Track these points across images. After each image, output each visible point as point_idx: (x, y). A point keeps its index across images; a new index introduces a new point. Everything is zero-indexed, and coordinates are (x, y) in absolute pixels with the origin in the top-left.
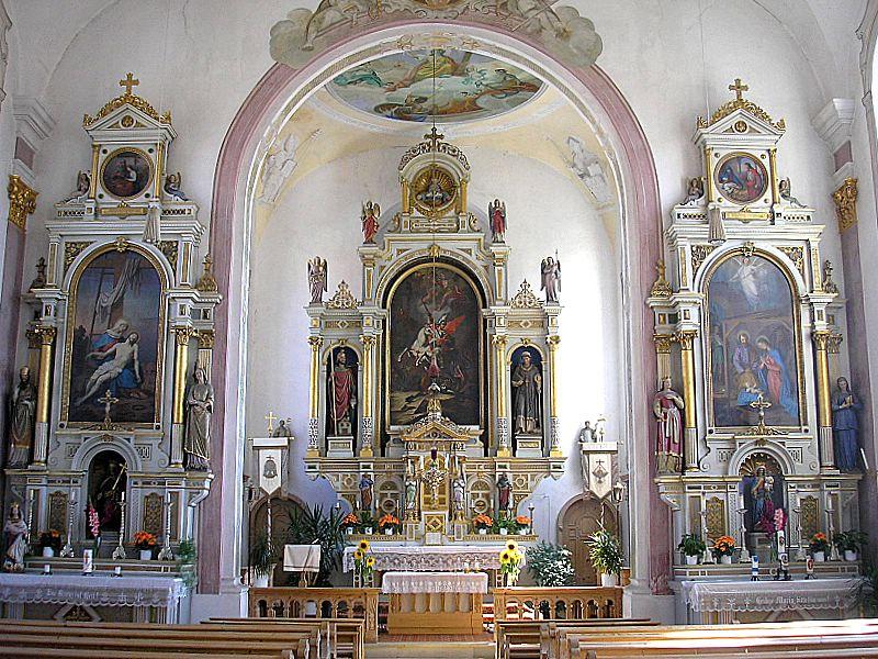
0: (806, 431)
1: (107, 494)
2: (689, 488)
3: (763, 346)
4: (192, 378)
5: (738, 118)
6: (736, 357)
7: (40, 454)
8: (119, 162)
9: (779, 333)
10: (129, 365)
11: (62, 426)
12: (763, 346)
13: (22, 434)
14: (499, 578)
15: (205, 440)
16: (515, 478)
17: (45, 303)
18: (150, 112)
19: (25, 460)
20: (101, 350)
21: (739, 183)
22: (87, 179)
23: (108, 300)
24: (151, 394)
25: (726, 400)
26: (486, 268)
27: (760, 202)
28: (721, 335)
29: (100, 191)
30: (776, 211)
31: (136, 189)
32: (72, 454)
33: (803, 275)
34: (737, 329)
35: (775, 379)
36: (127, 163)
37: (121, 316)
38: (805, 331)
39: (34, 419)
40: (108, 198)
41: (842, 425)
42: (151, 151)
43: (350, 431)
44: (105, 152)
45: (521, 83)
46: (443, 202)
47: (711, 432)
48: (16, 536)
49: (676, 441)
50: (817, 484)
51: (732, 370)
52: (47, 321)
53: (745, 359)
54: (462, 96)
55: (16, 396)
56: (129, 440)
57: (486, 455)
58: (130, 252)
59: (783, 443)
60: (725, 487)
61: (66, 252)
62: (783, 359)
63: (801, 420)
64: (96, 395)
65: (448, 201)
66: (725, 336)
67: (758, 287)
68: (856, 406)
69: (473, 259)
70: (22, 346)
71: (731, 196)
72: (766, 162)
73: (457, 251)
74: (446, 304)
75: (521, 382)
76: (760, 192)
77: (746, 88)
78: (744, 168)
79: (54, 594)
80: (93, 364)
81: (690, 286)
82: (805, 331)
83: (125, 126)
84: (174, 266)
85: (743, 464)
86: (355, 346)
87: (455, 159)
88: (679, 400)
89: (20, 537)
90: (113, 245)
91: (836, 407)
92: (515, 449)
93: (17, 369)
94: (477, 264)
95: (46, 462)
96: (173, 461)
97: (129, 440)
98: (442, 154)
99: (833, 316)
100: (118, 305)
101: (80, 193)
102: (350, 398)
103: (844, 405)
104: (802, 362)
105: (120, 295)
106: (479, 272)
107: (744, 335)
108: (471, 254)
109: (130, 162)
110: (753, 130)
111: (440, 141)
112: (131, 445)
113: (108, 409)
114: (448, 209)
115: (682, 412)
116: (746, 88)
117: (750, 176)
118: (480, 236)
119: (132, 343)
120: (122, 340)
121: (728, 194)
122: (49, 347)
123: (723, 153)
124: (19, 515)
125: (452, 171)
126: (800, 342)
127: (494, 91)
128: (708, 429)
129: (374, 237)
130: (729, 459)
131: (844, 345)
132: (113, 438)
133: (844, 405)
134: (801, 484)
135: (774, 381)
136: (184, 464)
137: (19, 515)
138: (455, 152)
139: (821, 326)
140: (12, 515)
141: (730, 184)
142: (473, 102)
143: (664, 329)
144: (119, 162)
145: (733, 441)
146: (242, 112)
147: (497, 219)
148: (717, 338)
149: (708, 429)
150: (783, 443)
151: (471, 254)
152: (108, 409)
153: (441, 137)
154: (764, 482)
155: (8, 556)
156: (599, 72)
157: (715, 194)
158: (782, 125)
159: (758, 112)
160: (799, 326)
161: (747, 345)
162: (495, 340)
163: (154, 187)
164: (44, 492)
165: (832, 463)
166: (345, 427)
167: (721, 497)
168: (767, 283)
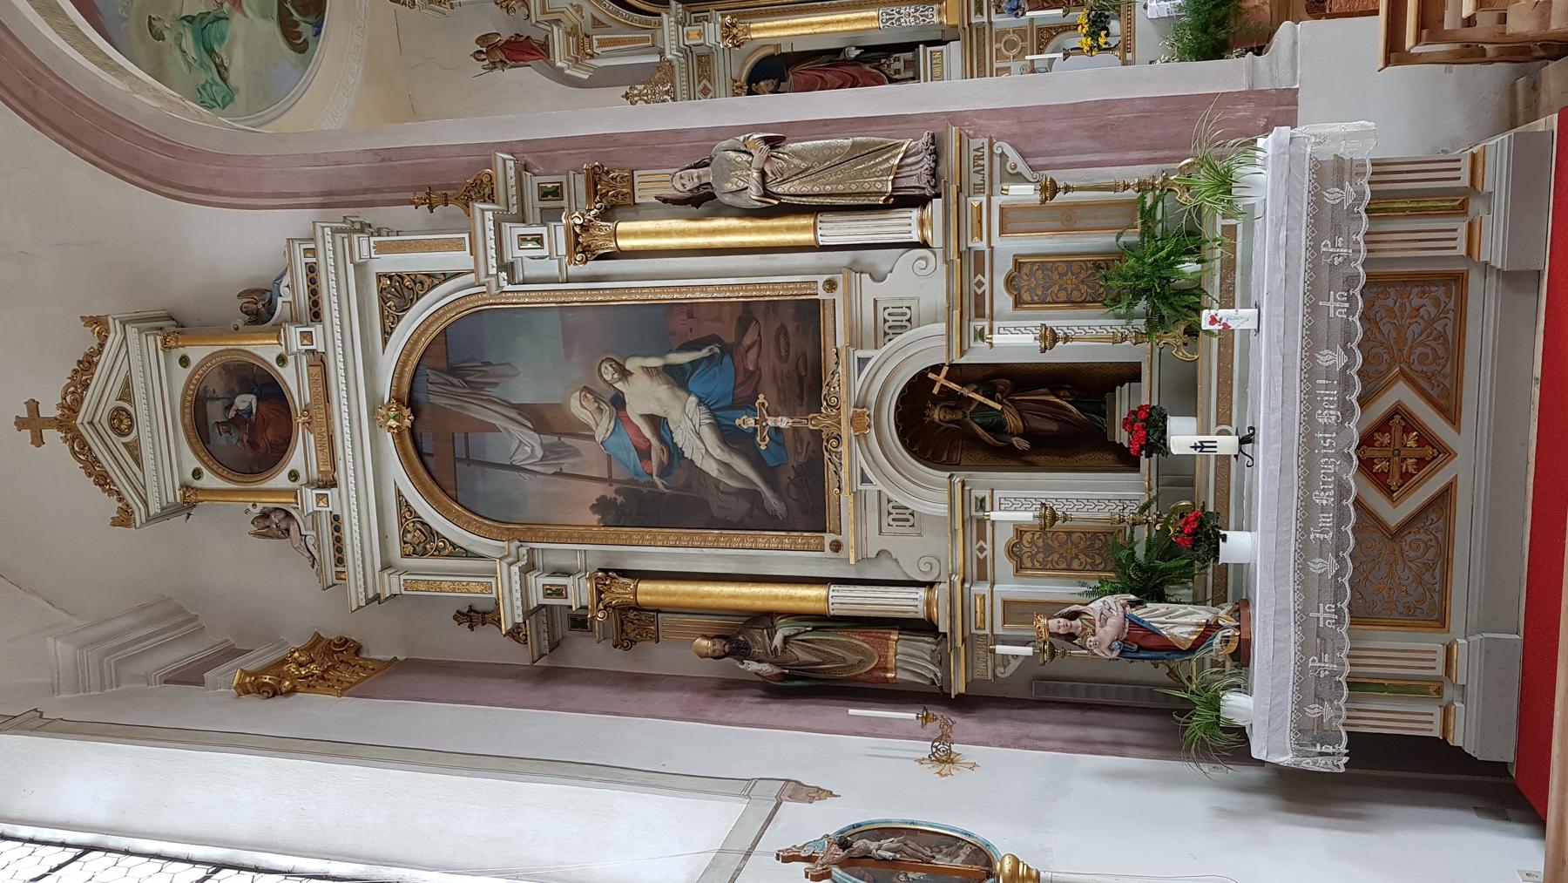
1: (1013, 421)
4: (701, 201)
7: (909, 602)
8: (220, 440)
10: (677, 377)
11: (837, 547)
13: (864, 652)
15: (854, 145)
17: (537, 598)
18: (87, 365)
19: (925, 645)
20: (644, 454)
22: (265, 515)
23: (526, 444)
24: (748, 313)
29: (280, 480)
31: (269, 389)
32: (905, 517)
36: (221, 420)
37: (560, 409)
39: (823, 621)
40: (296, 460)
42: (184, 361)
43: (909, 55)
44: (197, 474)
48: (1135, 624)
52: (579, 593)
55: (765, 668)
56: (863, 362)
58: (410, 400)
61: (423, 554)
64: (757, 461)
70: (660, 657)
77: (33, 406)
79: (1327, 520)
80: (679, 476)
83: (130, 427)
84: (435, 279)
86: (744, 64)
89: (1139, 613)
90: (398, 435)
93: (713, 669)
95: (930, 585)
96: (916, 238)
97: (863, 362)
100: (540, 418)
101: (293, 528)
102: (847, 62)
105: (513, 414)
109: (215, 411)
112: (875, 355)
113: (784, 422)
116: (33, 406)
119: (625, 374)
120: (619, 402)
122: (644, 586)
123: (191, 462)
124: (1073, 616)
129: (538, 36)
132: (861, 404)
136: (920, 202)
137: (1073, 616)
140: (1070, 637)
144: (220, 440)
146: (103, 159)
152: (784, 422)
155: (1193, 649)
163: (264, 350)
164: (1010, 587)
166: (900, 65)
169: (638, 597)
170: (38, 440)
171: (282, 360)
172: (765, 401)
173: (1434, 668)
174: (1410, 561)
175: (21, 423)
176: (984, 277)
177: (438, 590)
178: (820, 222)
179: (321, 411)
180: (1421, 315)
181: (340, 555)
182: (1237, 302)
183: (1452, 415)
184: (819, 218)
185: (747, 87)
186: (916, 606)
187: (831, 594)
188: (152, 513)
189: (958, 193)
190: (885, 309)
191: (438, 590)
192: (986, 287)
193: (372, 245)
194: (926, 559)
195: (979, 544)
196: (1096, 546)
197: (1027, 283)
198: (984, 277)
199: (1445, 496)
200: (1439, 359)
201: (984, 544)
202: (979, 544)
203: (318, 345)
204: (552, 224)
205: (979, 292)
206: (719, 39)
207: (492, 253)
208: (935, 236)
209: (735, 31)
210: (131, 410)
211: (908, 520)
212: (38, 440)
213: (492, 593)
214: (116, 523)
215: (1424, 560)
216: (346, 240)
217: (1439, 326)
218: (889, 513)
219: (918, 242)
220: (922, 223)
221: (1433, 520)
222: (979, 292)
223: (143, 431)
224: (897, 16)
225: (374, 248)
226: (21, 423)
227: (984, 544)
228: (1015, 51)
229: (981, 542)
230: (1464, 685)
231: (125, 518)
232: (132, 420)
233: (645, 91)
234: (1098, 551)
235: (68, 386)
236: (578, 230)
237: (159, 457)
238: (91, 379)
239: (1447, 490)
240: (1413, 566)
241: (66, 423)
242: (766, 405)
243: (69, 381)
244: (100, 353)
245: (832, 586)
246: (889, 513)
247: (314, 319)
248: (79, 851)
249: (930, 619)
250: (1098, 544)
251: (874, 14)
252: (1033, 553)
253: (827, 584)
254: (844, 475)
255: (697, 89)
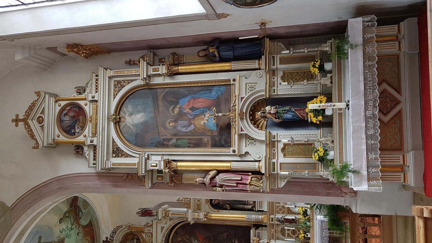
0: (234, 80)
2: (274, 171)
3: (177, 110)
5: (35, 121)
6: (184, 130)
9: (169, 99)
12: (177, 110)
14: (336, 233)
16: (278, 213)
21: (76, 122)
25: (213, 138)
26: (171, 219)
27: (87, 108)
28: (169, 140)
30: (90, 99)
33: (132, 81)
34: (165, 128)
35: (199, 102)
38: (168, 80)
41: (229, 54)
45: (71, 206)
46: (139, 239)
47: (234, 151)
49: (240, 178)
50: (273, 73)
51: (193, 133)
53: (185, 123)
54: (81, 235)
57: (266, 226)
59: (242, 98)
60: (275, 142)
62: (185, 96)
63: (227, 85)
65: (138, 237)
66: (169, 137)
67: (139, 112)
68: (216, 44)
69: (166, 226)
71: (83, 128)
72: (63, 103)
73: (162, 234)
74: (189, 240)
75: (228, 206)
76: (80, 108)
77: (17, 116)
78: (67, 118)
81: (136, 161)
82: (168, 80)
85: (258, 127)
87: (117, 232)
88: (212, 173)
91: (218, 59)
92: (263, 211)
94: (168, 224)
95: (260, 161)
98: (115, 238)
99: (160, 59)
103: (216, 53)
104: (187, 83)
106: (172, 223)
107: (169, 123)
108: (164, 227)
110: (43, 112)
111: (109, 239)
114: (142, 237)
115: (219, 172)
116: (17, 116)
117: (71, 114)
118: (155, 222)
121: (82, 130)
123: (57, 132)
125: (124, 233)
126: (174, 84)
127: (77, 218)
128: (232, 153)
130: (253, 139)
131: (179, 51)
133: (216, 53)
134: (272, 85)
135: (200, 103)
138: (114, 232)
139: (163, 69)
141: (76, 127)
142: (84, 227)
143: (167, 179)
145: (241, 136)
147: (146, 213)
148: (171, 143)
149: (232, 153)
150: (242, 98)
151: (164, 227)
153: (107, 238)
154: (270, 113)
156: (15, 206)
157: (81, 139)
158: (38, 94)
159: (31, 108)
160: (163, 84)
161: (176, 121)
162: (206, 219)
165: (257, 61)
167: (281, 146)
168: (137, 106)
169: (179, 71)
170: (17, 125)
171: (85, 136)
172: (215, 109)
173: (400, 162)
174: (391, 132)
175: (13, 121)
176: (275, 148)
177: (123, 73)
178: (232, 64)
179: (94, 123)
180: (388, 66)
181: (95, 149)
182: (343, 101)
183: (399, 91)
184: (232, 63)
185: (210, 201)
186: (256, 66)
187: (232, 65)
188: (44, 146)
189: (269, 159)
190: (248, 86)
191: (123, 73)
192: (276, 151)
193: (111, 164)
194: (258, 154)
195: (273, 149)
196: (306, 149)
197: (287, 78)
198: (275, 148)
199: (400, 112)
200: (394, 78)
201: (275, 149)
202: (273, 149)
203: (95, 143)
204: (160, 169)
205: (274, 80)
206: (203, 217)
207: (144, 167)
208: (263, 67)
209: (207, 216)
210: (43, 117)
211: (253, 87)
212: (17, 125)
213: (138, 70)
214: (34, 148)
215: (395, 132)
216: (104, 167)
217: (393, 69)
218: (248, 141)
219: (258, 68)
220: (259, 64)
221: (396, 121)
222: (274, 80)
223: (45, 123)
224: (250, 218)
225: (112, 165)
226: (13, 121)
227: (275, 149)
228: (281, 212)
229: (274, 148)
230: (409, 166)
231: (36, 147)
232: (43, 119)
233: (182, 200)
234: (306, 150)
235: (27, 110)
236: (167, 163)
237: (49, 133)
238: (34, 108)
239: (400, 111)
240: (392, 134)
241: (25, 120)
242: (216, 110)
243: (28, 109)
244: (37, 101)
245: (232, 62)
246: (248, 89)
247: (96, 93)
248: (21, 4)
249: (260, 171)
250: (306, 75)
251: (244, 216)
252: (288, 79)
253: (230, 162)
254: (237, 129)
255: (196, 200)
